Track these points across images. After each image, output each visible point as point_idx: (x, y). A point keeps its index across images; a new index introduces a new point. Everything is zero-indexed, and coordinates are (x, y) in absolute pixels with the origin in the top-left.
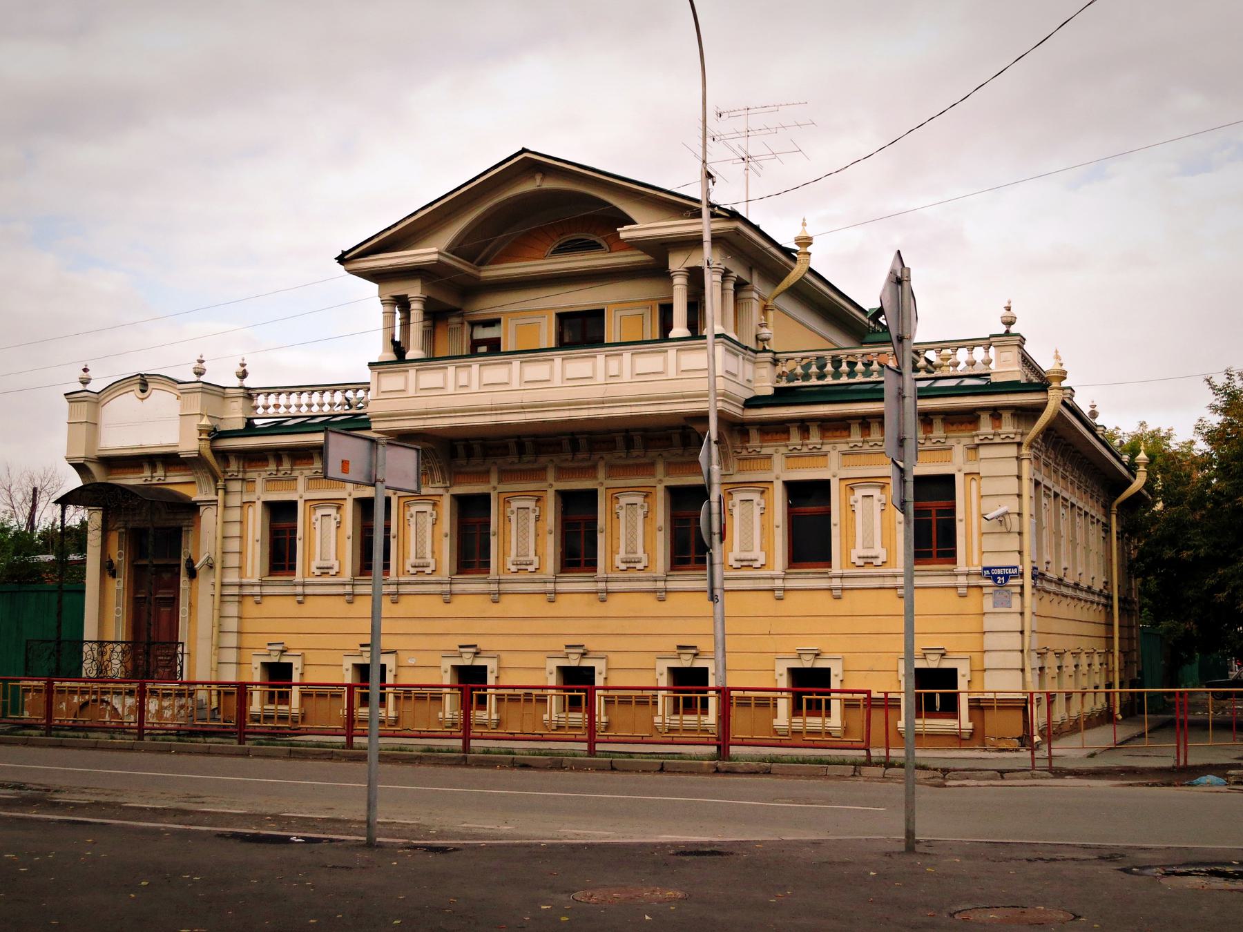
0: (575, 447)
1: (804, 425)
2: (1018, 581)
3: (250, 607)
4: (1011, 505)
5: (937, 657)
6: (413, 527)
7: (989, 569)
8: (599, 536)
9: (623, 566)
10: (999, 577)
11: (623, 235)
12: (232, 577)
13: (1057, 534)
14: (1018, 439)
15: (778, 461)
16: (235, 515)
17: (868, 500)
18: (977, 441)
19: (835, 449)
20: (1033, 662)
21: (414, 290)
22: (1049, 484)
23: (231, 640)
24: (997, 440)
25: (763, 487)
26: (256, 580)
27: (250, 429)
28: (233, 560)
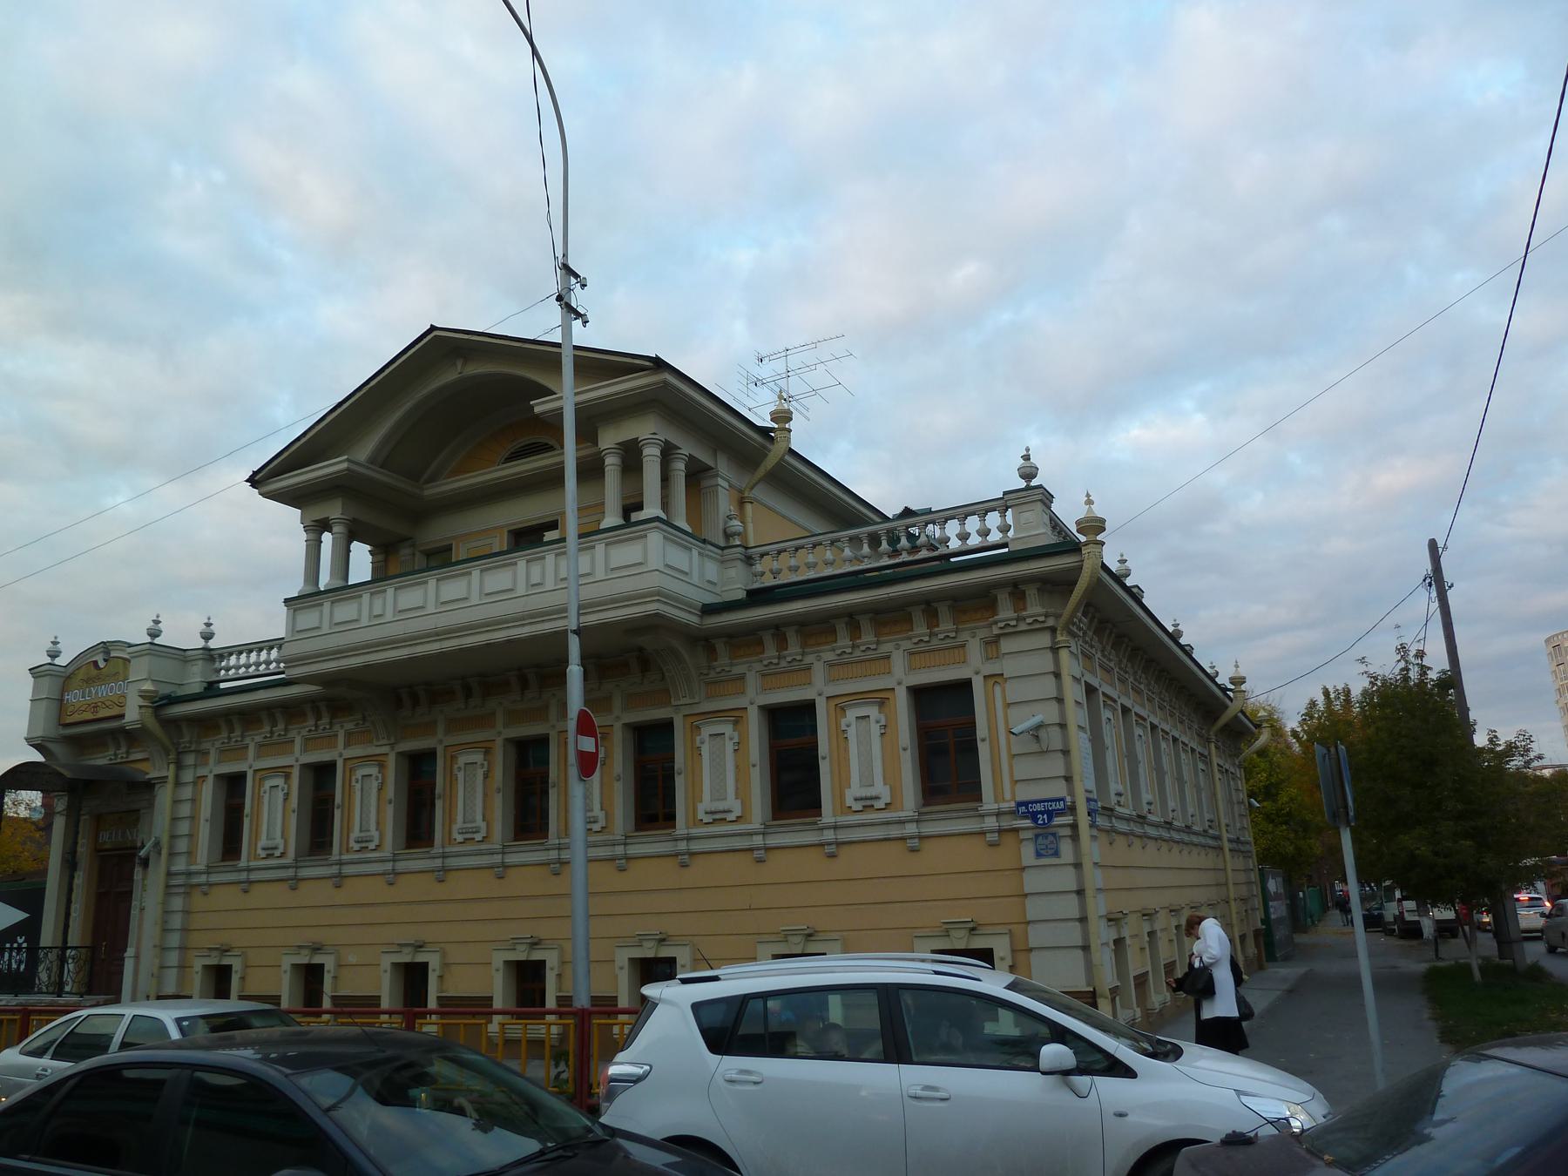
0: (524, 684)
1: (778, 629)
2: (1068, 819)
3: (198, 901)
4: (1049, 714)
5: (963, 933)
6: (358, 794)
7: (1025, 804)
8: (980, 745)
9: (357, 846)
10: (1043, 820)
11: (537, 410)
12: (180, 865)
13: (1180, 780)
14: (1051, 622)
15: (752, 681)
16: (187, 792)
17: (864, 722)
18: (996, 631)
19: (819, 660)
20: (1102, 934)
21: (334, 510)
22: (1167, 728)
23: (174, 940)
24: (1023, 627)
25: (736, 717)
26: (202, 867)
27: (211, 690)
28: (182, 845)
